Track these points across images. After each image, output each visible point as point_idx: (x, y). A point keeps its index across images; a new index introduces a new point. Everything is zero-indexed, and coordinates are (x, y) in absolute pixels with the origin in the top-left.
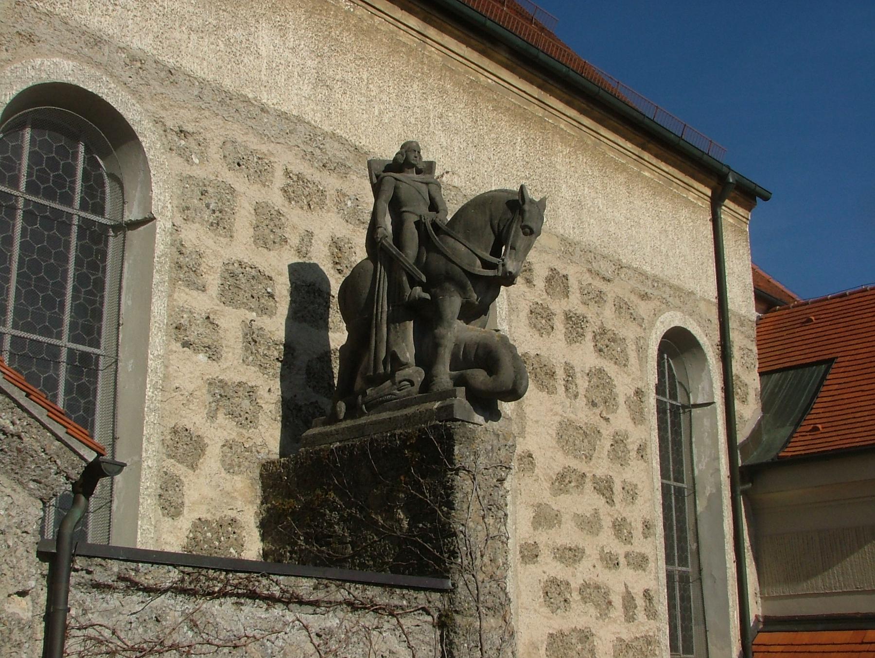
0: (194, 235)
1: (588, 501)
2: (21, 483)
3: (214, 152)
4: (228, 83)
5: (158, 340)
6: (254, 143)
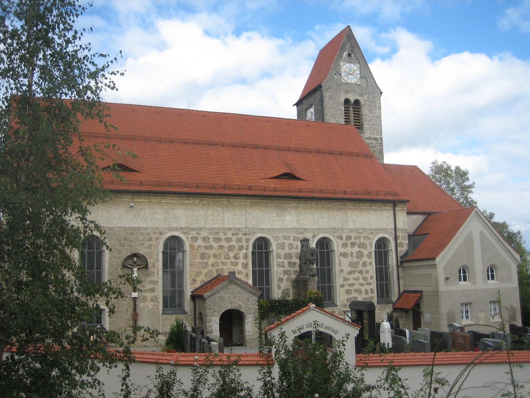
0: (279, 251)
1: (357, 275)
3: (281, 238)
4: (282, 227)
5: (275, 267)
6: (287, 234)
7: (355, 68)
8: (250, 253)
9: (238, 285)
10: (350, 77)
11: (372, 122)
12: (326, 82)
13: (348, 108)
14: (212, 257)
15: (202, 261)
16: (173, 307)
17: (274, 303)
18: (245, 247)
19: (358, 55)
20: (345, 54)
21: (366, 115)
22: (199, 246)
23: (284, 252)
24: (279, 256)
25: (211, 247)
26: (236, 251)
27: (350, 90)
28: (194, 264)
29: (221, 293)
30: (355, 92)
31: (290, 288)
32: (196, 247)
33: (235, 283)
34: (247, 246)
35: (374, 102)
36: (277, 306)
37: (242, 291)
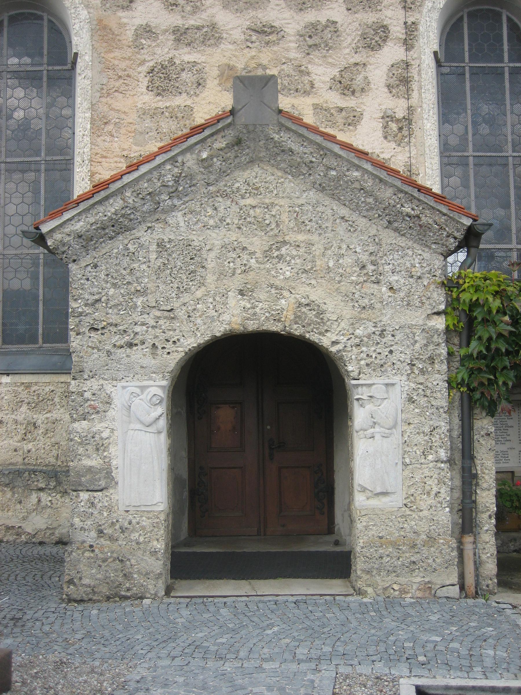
2: (427, 246)
8: (428, 63)
9: (297, 168)
14: (212, 84)
15: (162, 103)
16: (21, 340)
18: (397, 30)
22: (147, 31)
25: (211, 35)
26: (345, 54)
28: (113, 116)
29: (178, 218)
32: (130, 34)
33: (277, 154)
34: (411, 30)
37: (331, 208)
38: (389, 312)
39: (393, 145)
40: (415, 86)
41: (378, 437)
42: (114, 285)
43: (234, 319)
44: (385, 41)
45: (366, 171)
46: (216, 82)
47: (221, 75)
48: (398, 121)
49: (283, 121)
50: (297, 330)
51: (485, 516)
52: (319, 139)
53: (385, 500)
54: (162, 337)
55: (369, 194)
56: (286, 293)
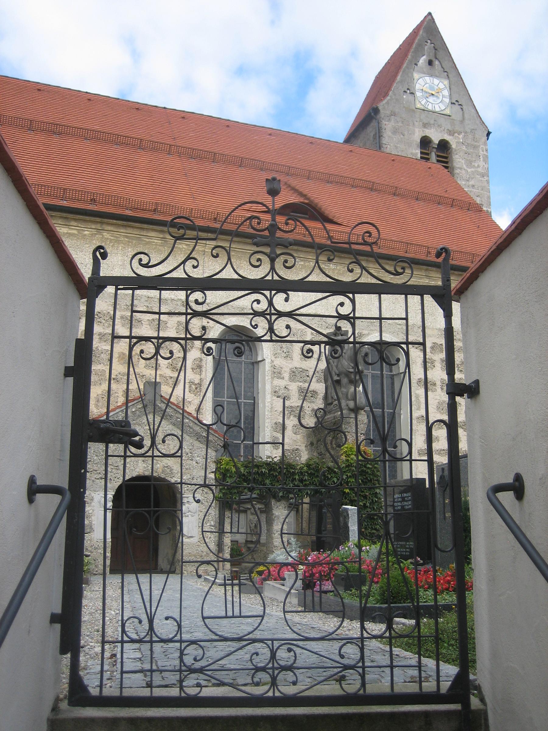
7: (441, 86)
10: (431, 99)
11: (471, 183)
12: (388, 103)
13: (428, 154)
17: (257, 466)
19: (446, 64)
20: (423, 60)
21: (461, 169)
23: (291, 366)
24: (277, 373)
27: (432, 122)
30: (440, 126)
31: (303, 448)
35: (475, 147)
36: (263, 474)
38: (195, 471)
39: (193, 395)
40: (204, 369)
41: (190, 516)
42: (97, 456)
43: (140, 471)
44: (192, 348)
45: (191, 420)
46: (117, 360)
47: (119, 357)
48: (196, 384)
49: (163, 400)
50: (163, 476)
51: (227, 547)
52: (175, 407)
53: (192, 539)
54: (114, 476)
55: (191, 428)
56: (159, 462)
